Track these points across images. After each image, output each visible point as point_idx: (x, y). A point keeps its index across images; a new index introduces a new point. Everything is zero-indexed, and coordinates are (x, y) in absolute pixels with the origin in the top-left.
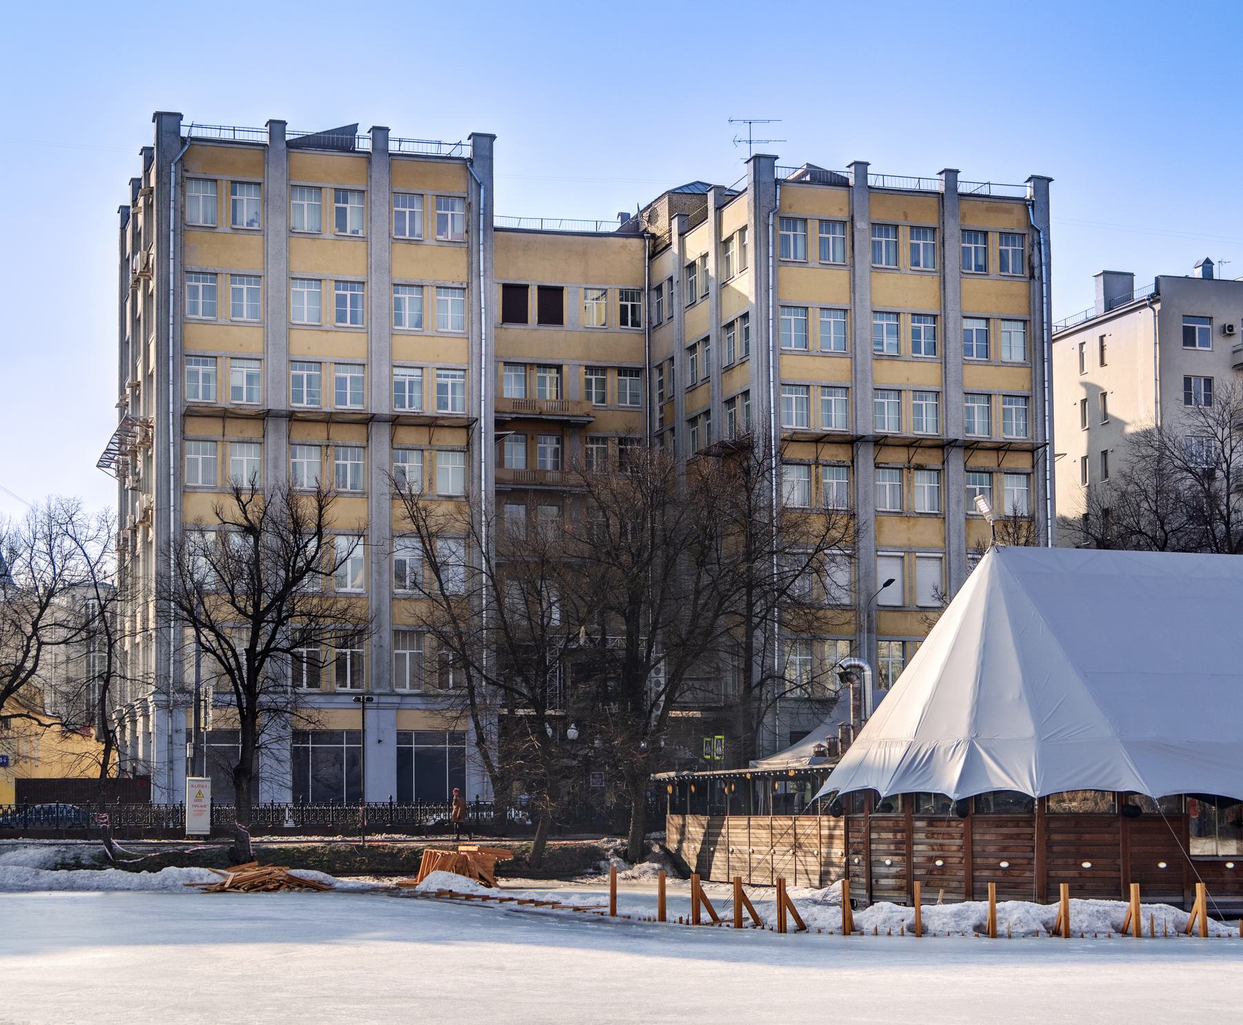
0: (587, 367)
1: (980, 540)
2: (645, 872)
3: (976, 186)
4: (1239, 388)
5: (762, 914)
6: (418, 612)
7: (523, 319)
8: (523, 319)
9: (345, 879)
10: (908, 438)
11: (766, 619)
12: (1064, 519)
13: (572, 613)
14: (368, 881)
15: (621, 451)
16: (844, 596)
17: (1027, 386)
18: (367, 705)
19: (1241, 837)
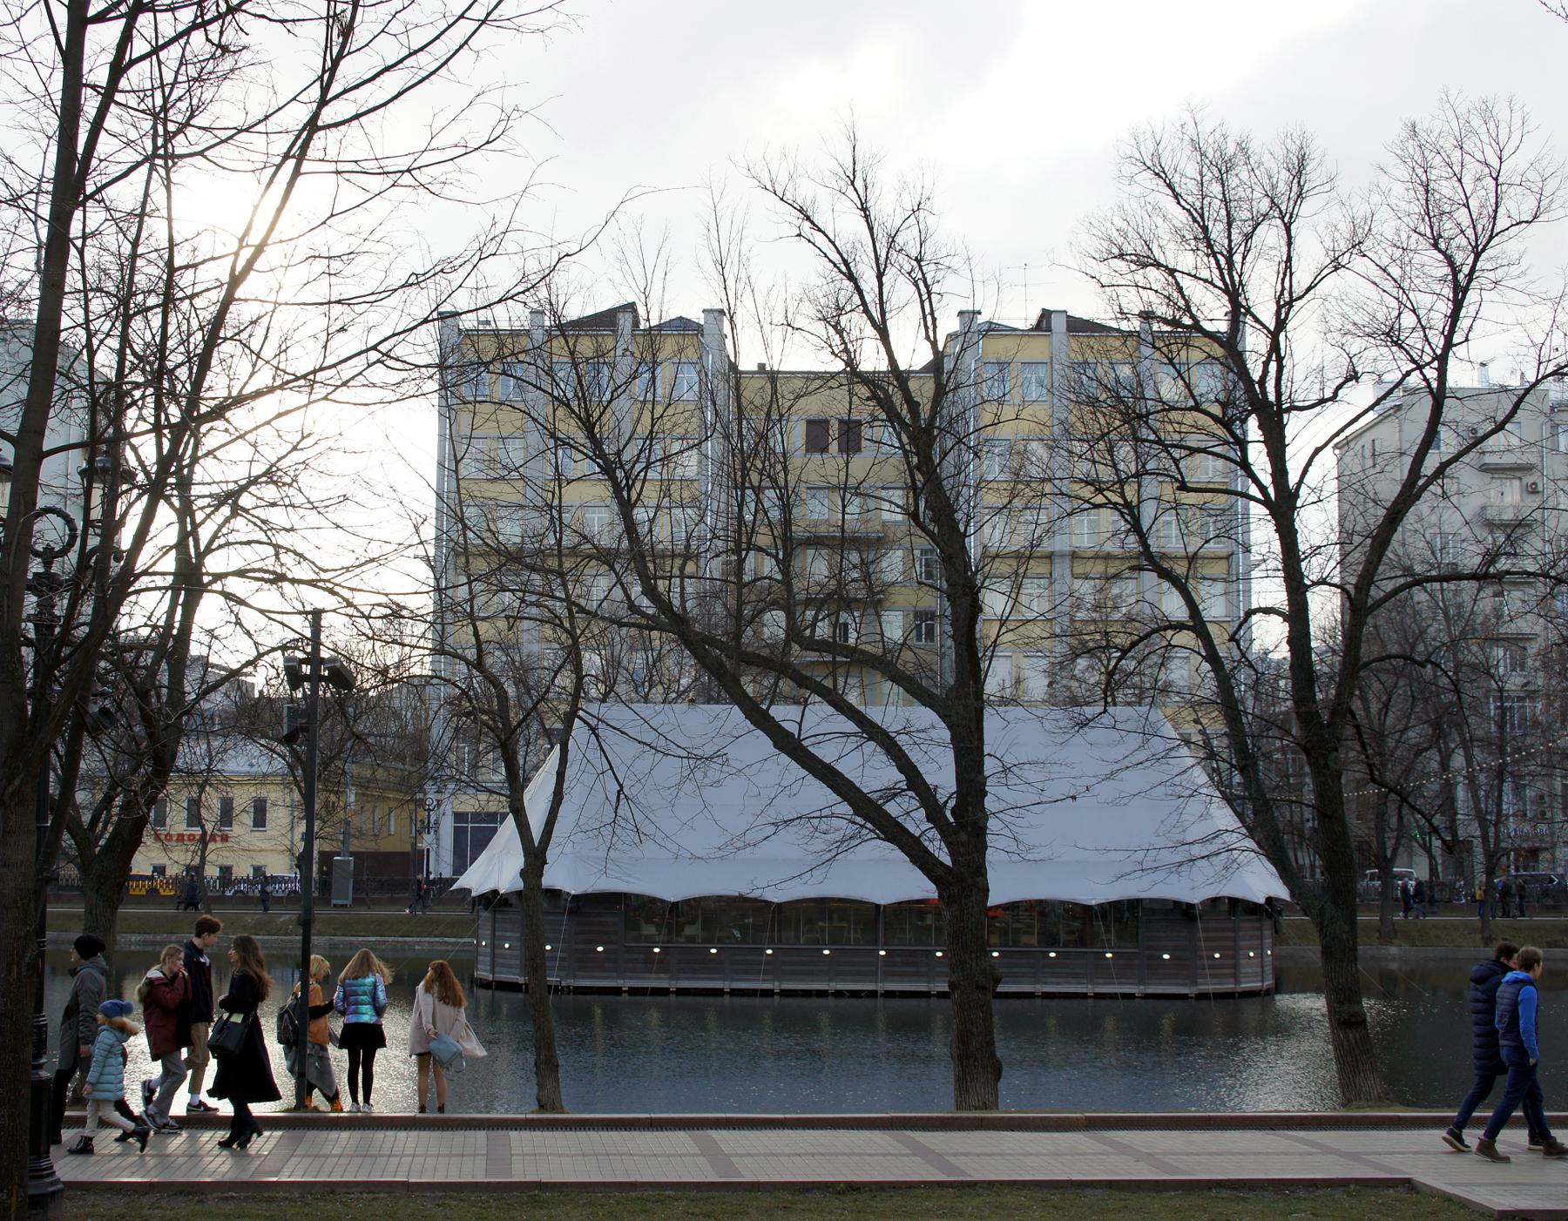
0: (511, 905)
1: (245, 56)
2: (81, 397)
3: (411, 158)
4: (215, 1195)
5: (431, 347)
6: (1533, 643)
7: (824, 450)
8: (824, 450)
9: (1460, 804)
10: (1343, 605)
11: (236, 511)
12: (555, 894)
13: (554, 710)
14: (729, 343)
15: (39, 828)
16: (247, 838)
17: (415, 1101)
18: (320, 912)
19: (2, 320)
